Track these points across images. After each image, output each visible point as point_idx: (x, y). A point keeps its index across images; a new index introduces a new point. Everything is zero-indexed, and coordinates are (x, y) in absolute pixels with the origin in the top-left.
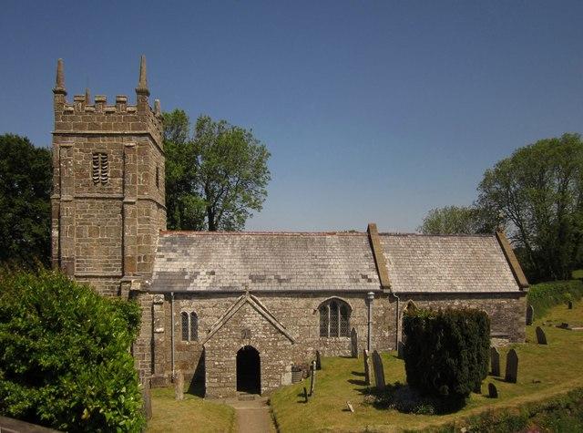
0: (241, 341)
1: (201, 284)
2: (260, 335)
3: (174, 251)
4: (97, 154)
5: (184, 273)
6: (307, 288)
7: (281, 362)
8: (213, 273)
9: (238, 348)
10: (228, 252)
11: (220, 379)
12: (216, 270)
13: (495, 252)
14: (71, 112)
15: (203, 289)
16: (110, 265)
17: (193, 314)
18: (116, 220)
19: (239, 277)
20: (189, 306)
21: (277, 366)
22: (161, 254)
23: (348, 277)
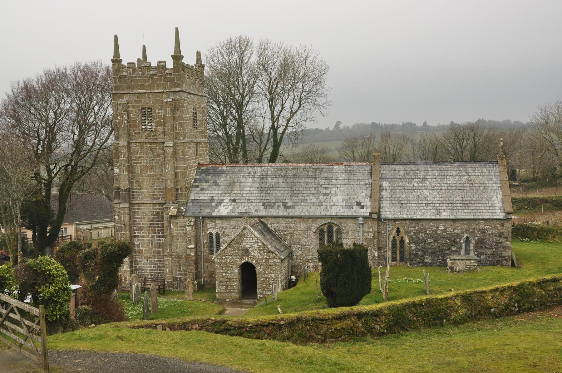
0: (241, 258)
1: (223, 211)
2: (256, 254)
3: (207, 181)
4: (144, 109)
5: (212, 200)
6: (307, 214)
7: (273, 275)
8: (234, 201)
9: (240, 264)
10: (249, 182)
11: (227, 286)
12: (237, 198)
13: (491, 179)
14: (125, 77)
15: (224, 214)
16: (156, 195)
17: (217, 234)
18: (160, 160)
19: (254, 204)
20: (214, 228)
21: (269, 278)
22: (197, 184)
23: (344, 204)
